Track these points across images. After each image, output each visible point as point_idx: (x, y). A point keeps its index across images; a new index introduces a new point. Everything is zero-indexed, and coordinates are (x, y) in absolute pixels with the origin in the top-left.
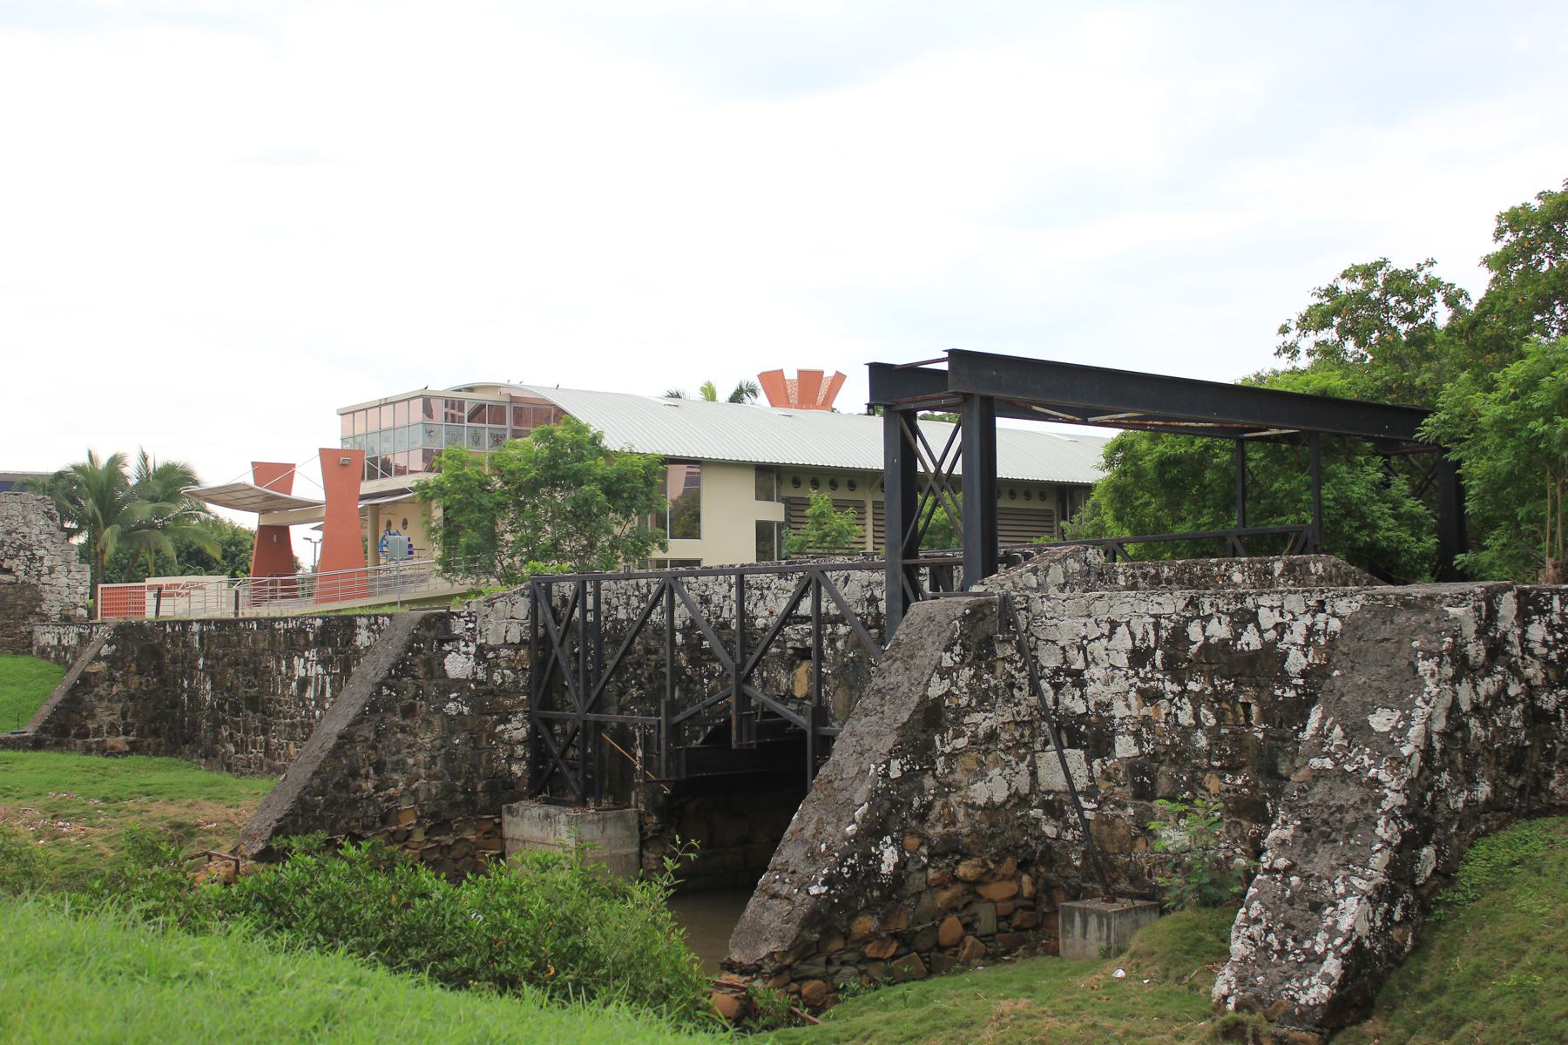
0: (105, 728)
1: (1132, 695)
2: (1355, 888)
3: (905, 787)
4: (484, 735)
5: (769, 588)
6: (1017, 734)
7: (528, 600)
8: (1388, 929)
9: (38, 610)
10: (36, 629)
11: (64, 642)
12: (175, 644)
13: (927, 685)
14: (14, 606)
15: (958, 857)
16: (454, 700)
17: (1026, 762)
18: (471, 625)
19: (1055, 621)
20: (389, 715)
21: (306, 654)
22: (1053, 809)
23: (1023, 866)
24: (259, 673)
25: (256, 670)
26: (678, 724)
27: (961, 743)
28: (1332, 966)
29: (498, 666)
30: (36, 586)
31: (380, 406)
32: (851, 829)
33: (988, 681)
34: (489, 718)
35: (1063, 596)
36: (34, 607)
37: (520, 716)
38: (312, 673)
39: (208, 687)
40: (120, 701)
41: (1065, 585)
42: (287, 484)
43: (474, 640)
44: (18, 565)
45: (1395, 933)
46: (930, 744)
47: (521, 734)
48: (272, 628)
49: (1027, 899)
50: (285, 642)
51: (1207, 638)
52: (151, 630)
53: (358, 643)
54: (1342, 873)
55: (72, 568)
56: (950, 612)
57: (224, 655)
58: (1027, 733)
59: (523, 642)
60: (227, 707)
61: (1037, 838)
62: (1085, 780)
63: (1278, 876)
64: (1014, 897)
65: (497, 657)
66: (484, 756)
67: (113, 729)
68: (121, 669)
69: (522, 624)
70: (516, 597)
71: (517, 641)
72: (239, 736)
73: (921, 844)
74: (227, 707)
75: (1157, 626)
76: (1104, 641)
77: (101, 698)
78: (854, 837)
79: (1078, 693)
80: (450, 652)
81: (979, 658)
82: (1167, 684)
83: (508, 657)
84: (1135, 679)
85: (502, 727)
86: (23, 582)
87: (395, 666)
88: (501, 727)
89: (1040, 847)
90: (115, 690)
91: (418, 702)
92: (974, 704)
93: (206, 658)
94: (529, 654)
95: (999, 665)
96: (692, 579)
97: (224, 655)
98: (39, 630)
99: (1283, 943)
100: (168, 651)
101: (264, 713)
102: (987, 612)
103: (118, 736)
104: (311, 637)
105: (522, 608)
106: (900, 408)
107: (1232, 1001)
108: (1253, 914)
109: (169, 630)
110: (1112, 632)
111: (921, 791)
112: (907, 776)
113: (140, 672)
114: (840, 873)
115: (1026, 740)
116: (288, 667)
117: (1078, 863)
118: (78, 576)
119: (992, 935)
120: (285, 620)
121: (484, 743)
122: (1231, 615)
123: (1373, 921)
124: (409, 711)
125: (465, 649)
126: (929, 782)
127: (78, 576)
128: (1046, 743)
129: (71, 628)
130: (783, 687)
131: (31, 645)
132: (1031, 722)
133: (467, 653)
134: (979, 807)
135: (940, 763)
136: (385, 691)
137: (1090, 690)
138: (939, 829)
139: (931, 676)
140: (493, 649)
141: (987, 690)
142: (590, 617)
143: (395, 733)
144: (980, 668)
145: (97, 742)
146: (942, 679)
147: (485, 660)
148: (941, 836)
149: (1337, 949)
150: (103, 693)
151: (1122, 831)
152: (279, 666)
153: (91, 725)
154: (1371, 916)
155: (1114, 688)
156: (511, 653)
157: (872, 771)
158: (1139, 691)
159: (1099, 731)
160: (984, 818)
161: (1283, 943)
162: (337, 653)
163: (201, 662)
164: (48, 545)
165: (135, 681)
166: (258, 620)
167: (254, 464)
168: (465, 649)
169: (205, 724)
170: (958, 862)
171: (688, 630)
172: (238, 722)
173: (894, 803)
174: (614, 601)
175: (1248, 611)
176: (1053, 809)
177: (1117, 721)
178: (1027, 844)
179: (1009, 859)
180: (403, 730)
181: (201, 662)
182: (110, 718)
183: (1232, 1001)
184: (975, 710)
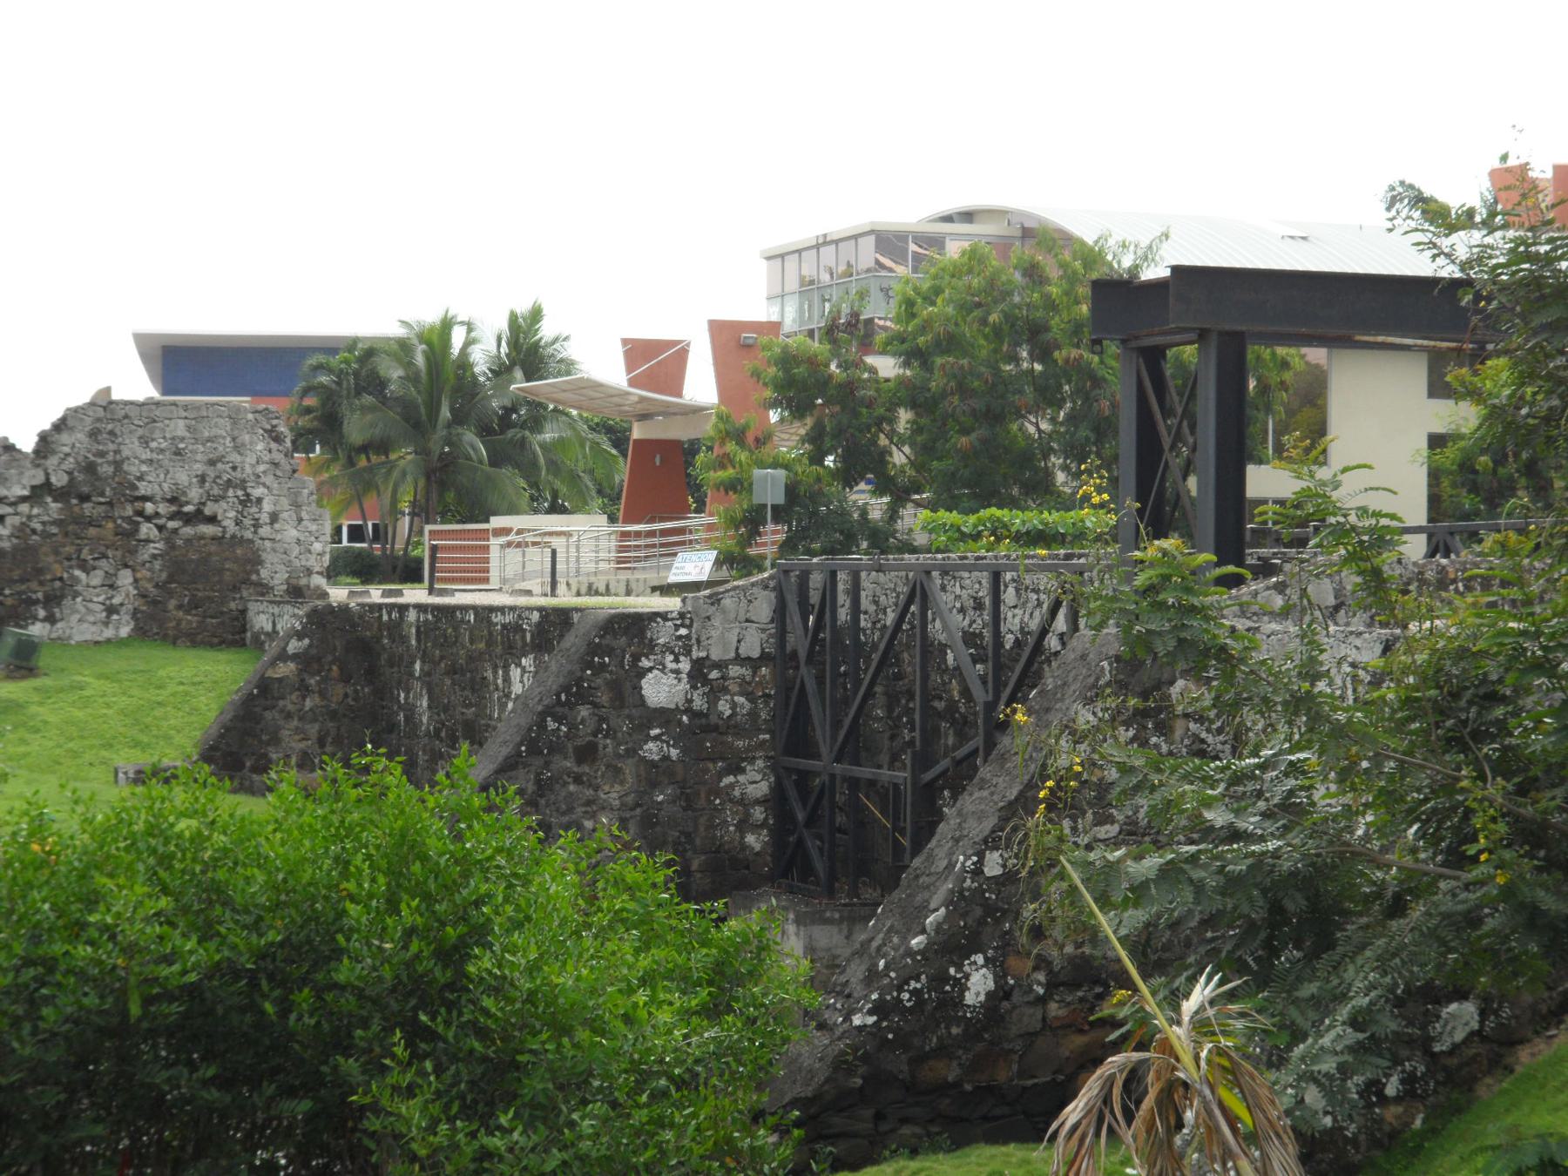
7: (773, 595)
8: (1370, 1105)
14: (221, 571)
16: (657, 738)
18: (683, 631)
21: (523, 660)
26: (930, 784)
27: (1111, 830)
30: (251, 541)
31: (817, 247)
32: (917, 942)
33: (1157, 746)
34: (711, 766)
37: (760, 763)
39: (425, 704)
40: (315, 720)
41: (1337, 608)
43: (688, 653)
44: (227, 513)
47: (762, 789)
50: (503, 643)
52: (361, 617)
55: (304, 515)
56: (1104, 650)
57: (442, 658)
59: (764, 658)
60: (443, 734)
65: (723, 678)
66: (702, 820)
68: (319, 672)
69: (763, 630)
70: (755, 590)
71: (756, 654)
74: (443, 734)
77: (289, 716)
78: (919, 952)
80: (650, 669)
83: (742, 678)
85: (731, 779)
86: (233, 537)
87: (566, 689)
90: (308, 703)
93: (423, 662)
96: (966, 575)
97: (442, 658)
98: (253, 607)
105: (763, 608)
113: (346, 678)
114: (899, 1000)
118: (313, 527)
121: (702, 802)
124: (587, 753)
125: (674, 666)
127: (313, 527)
131: (244, 630)
133: (677, 672)
136: (551, 724)
140: (720, 665)
143: (565, 784)
144: (1145, 728)
147: (706, 681)
150: (290, 707)
152: (496, 678)
157: (959, 865)
163: (417, 666)
164: (269, 480)
165: (338, 690)
167: (625, 342)
168: (674, 666)
173: (989, 909)
180: (578, 780)
181: (417, 666)
182: (302, 745)
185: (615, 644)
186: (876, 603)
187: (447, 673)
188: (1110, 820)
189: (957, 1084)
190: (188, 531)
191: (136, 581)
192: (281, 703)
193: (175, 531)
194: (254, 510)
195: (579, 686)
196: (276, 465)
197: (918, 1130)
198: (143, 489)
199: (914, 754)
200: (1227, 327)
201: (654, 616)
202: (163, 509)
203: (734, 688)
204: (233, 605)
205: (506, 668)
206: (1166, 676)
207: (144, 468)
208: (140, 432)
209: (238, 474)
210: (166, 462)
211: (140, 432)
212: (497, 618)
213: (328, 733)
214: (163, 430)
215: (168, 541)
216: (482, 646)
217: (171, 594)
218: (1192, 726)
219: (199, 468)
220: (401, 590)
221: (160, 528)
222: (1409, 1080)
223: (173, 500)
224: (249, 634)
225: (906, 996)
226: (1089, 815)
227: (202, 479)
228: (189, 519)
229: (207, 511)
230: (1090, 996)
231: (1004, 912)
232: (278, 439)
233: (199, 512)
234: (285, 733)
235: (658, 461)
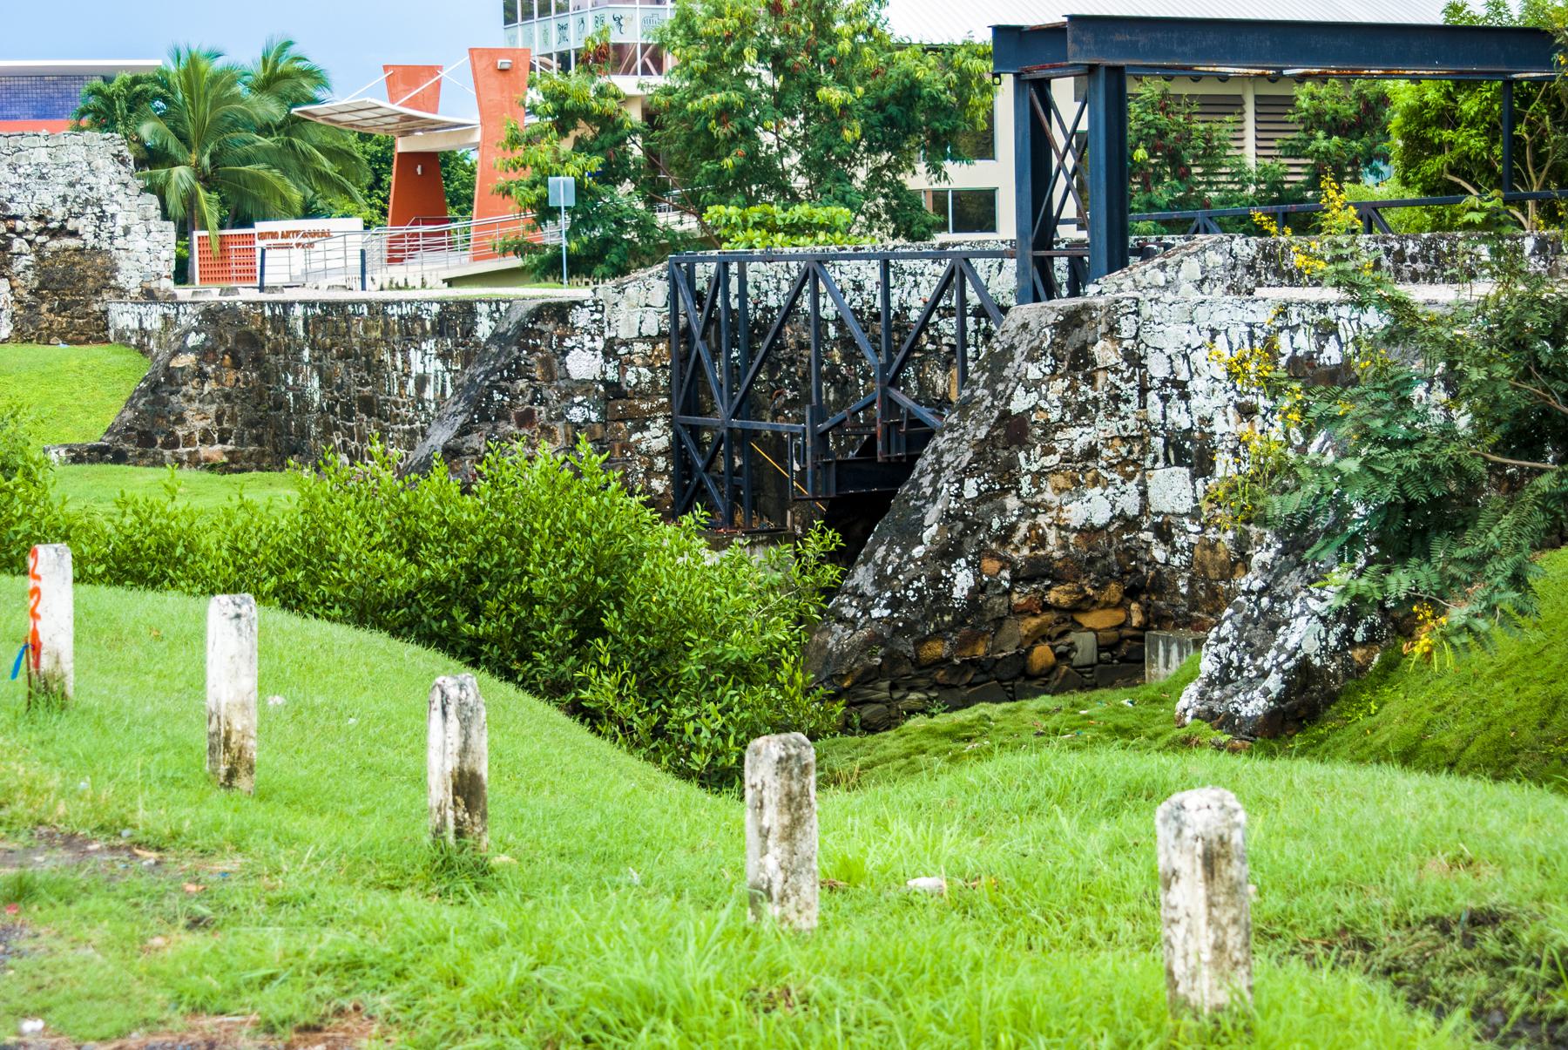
0: (197, 436)
1: (1230, 409)
2: (1308, 608)
3: (984, 508)
4: (617, 445)
5: (922, 274)
6: (1124, 451)
7: (666, 284)
8: (1345, 649)
9: (112, 282)
10: (111, 307)
11: (146, 325)
12: (276, 330)
13: (1009, 399)
15: (1048, 582)
16: (579, 404)
17: (1135, 481)
18: (597, 316)
19: (1161, 327)
20: (502, 424)
21: (424, 345)
22: (1164, 533)
23: (1132, 593)
24: (375, 368)
25: (368, 364)
27: (1052, 460)
28: (1274, 683)
29: (632, 363)
30: (108, 251)
32: (918, 552)
35: (1199, 297)
36: (108, 279)
37: (661, 422)
38: (430, 370)
39: (316, 383)
40: (213, 402)
41: (1202, 281)
42: (431, 99)
43: (602, 333)
44: (85, 226)
45: (1358, 654)
46: (1012, 463)
47: (662, 443)
48: (385, 313)
49: (1135, 628)
50: (400, 331)
51: (1295, 350)
53: (479, 334)
54: (1303, 594)
55: (152, 227)
57: (333, 345)
58: (1136, 449)
59: (662, 335)
60: (338, 409)
61: (1148, 564)
62: (1190, 501)
63: (1254, 598)
64: (1121, 626)
65: (630, 353)
67: (206, 438)
68: (214, 362)
70: (652, 280)
71: (654, 333)
72: (353, 444)
73: (1002, 568)
74: (338, 409)
75: (1252, 336)
76: (1205, 352)
77: (190, 399)
78: (921, 559)
79: (1183, 407)
80: (573, 348)
81: (1074, 367)
82: (1261, 398)
84: (1233, 393)
88: (636, 436)
89: (1151, 573)
90: (207, 388)
91: (536, 407)
92: (1068, 418)
93: (312, 348)
94: (669, 348)
95: (1101, 376)
97: (333, 345)
98: (115, 309)
99: (1241, 660)
100: (269, 339)
101: (379, 416)
102: (1085, 317)
103: (213, 444)
104: (428, 326)
106: (1031, 76)
107: (1190, 713)
108: (1223, 633)
109: (268, 313)
110: (1213, 340)
111: (1002, 510)
112: (983, 497)
113: (237, 364)
115: (1135, 456)
116: (404, 362)
117: (1184, 590)
118: (160, 237)
119: (1091, 665)
120: (399, 303)
122: (1316, 326)
123: (1325, 639)
125: (591, 345)
126: (1012, 502)
128: (1156, 460)
129: (154, 307)
130: (940, 391)
131: (106, 328)
132: (1141, 438)
133: (594, 349)
134: (1075, 530)
135: (1025, 482)
136: (497, 396)
137: (1194, 403)
138: (1025, 551)
139: (1014, 389)
140: (625, 343)
141: (1084, 403)
142: (735, 304)
145: (190, 454)
146: (1027, 392)
147: (617, 357)
148: (1027, 559)
149: (1279, 665)
150: (193, 392)
151: (1222, 556)
153: (181, 432)
154: (1323, 635)
155: (1215, 401)
156: (647, 347)
158: (1238, 406)
159: (1202, 447)
160: (1081, 541)
161: (1241, 660)
162: (457, 345)
164: (120, 198)
165: (230, 376)
166: (368, 303)
168: (591, 345)
169: (314, 430)
170: (1048, 588)
171: (840, 322)
172: (351, 429)
173: (969, 525)
174: (764, 286)
175: (1329, 323)
176: (1164, 533)
177: (1217, 438)
178: (1136, 569)
179: (1113, 586)
181: (306, 353)
183: (1190, 713)
184: (1068, 425)
185: (544, 328)
186: (758, 288)
187: (340, 358)
188: (1053, 451)
189: (948, 660)
190: (54, 245)
191: (13, 289)
192: (184, 388)
193: (43, 245)
194: (109, 224)
195: (518, 364)
196: (126, 185)
197: (921, 696)
198: (14, 209)
199: (812, 409)
200: (1111, 63)
201: (573, 304)
202: (32, 226)
203: (638, 361)
204: (96, 307)
205: (405, 352)
206: (1090, 339)
207: (14, 191)
208: (9, 159)
209: (94, 194)
210: (32, 186)
211: (9, 159)
212: (393, 311)
213: (224, 413)
214: (28, 158)
215: (37, 253)
216: (377, 334)
217: (43, 298)
218: (1111, 377)
219: (61, 190)
220: (235, 289)
221: (30, 243)
222: (1371, 629)
223: (40, 218)
224: (112, 332)
225: (910, 593)
226: (1038, 449)
227: (64, 199)
228: (54, 234)
229: (70, 226)
230: (1041, 588)
231: (979, 525)
232: (123, 162)
233: (62, 227)
234: (188, 414)
235: (419, 170)
